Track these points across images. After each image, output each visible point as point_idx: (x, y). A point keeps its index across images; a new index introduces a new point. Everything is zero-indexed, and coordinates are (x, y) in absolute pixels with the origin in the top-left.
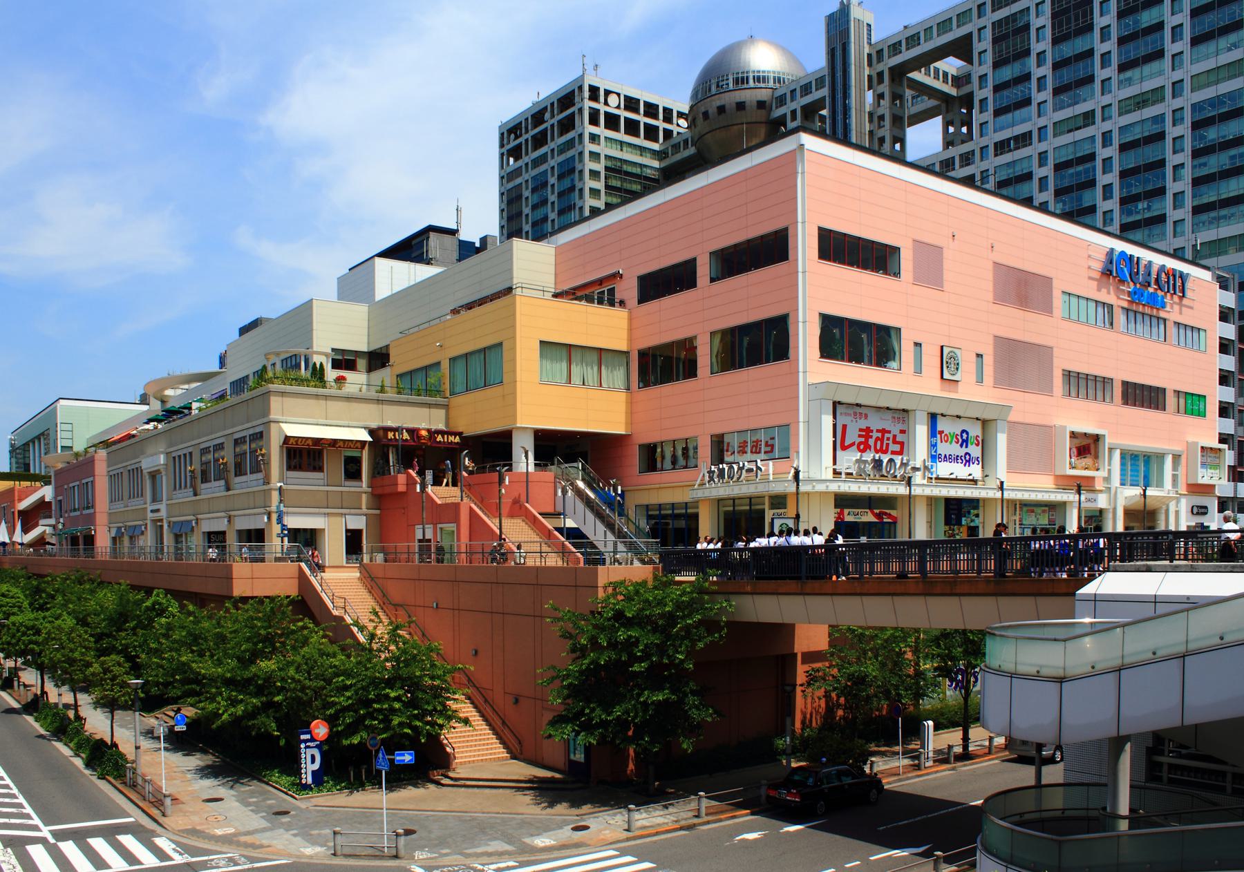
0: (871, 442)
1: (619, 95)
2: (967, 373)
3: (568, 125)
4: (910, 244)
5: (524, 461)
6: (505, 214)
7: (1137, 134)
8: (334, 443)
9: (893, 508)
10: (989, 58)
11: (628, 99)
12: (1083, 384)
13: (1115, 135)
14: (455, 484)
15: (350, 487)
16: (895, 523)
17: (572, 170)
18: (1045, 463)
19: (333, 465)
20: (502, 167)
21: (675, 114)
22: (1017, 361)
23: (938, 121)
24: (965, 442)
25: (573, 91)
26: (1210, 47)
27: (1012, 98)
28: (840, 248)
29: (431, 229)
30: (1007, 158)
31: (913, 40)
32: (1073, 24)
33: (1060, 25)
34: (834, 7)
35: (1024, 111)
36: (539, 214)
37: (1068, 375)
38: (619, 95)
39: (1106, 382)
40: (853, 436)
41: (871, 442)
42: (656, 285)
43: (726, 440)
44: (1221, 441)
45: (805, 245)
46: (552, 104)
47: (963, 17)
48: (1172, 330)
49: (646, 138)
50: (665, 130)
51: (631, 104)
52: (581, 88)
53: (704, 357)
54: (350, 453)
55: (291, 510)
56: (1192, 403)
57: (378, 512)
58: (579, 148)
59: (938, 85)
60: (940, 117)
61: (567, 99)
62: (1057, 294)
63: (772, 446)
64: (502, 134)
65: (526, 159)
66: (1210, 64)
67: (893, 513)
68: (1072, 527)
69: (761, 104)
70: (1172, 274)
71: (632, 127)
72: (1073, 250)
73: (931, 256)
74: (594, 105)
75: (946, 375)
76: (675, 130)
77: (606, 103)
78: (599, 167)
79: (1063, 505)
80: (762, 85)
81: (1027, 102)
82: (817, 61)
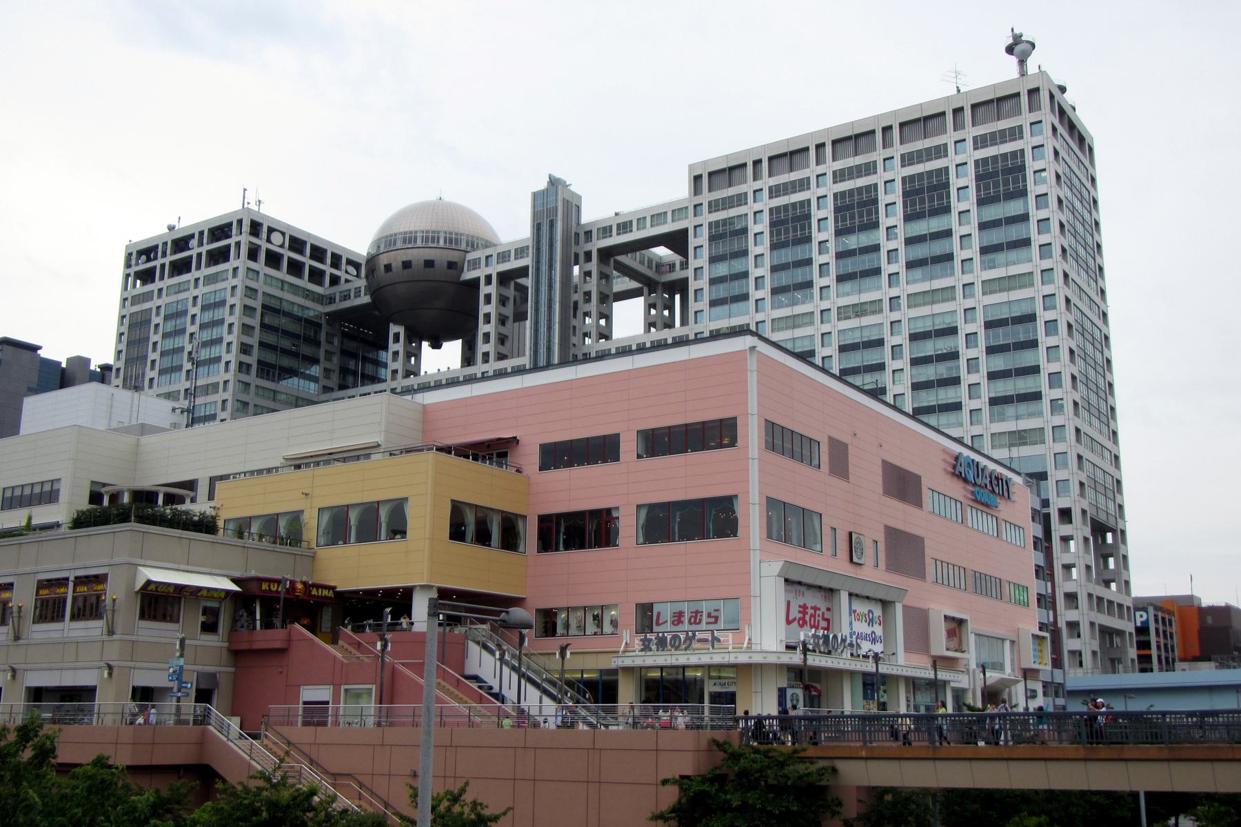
0: (807, 618)
1: (283, 234)
2: (868, 558)
4: (826, 441)
6: (124, 338)
8: (196, 591)
9: (819, 681)
10: (705, 253)
15: (210, 640)
16: (819, 696)
20: (126, 288)
21: (344, 261)
24: (871, 622)
25: (231, 224)
31: (625, 227)
32: (791, 234)
34: (542, 185)
35: (741, 305)
36: (169, 344)
38: (283, 234)
41: (807, 618)
43: (656, 609)
44: (1041, 629)
45: (752, 435)
46: (201, 233)
47: (679, 212)
50: (332, 275)
51: (297, 244)
52: (240, 222)
53: (628, 526)
54: (210, 604)
55: (138, 664)
57: (232, 669)
60: (642, 299)
63: (717, 618)
64: (130, 254)
65: (158, 284)
66: (925, 286)
67: (818, 686)
71: (295, 268)
73: (839, 452)
75: (855, 559)
76: (344, 276)
77: (269, 240)
80: (454, 246)
81: (745, 297)
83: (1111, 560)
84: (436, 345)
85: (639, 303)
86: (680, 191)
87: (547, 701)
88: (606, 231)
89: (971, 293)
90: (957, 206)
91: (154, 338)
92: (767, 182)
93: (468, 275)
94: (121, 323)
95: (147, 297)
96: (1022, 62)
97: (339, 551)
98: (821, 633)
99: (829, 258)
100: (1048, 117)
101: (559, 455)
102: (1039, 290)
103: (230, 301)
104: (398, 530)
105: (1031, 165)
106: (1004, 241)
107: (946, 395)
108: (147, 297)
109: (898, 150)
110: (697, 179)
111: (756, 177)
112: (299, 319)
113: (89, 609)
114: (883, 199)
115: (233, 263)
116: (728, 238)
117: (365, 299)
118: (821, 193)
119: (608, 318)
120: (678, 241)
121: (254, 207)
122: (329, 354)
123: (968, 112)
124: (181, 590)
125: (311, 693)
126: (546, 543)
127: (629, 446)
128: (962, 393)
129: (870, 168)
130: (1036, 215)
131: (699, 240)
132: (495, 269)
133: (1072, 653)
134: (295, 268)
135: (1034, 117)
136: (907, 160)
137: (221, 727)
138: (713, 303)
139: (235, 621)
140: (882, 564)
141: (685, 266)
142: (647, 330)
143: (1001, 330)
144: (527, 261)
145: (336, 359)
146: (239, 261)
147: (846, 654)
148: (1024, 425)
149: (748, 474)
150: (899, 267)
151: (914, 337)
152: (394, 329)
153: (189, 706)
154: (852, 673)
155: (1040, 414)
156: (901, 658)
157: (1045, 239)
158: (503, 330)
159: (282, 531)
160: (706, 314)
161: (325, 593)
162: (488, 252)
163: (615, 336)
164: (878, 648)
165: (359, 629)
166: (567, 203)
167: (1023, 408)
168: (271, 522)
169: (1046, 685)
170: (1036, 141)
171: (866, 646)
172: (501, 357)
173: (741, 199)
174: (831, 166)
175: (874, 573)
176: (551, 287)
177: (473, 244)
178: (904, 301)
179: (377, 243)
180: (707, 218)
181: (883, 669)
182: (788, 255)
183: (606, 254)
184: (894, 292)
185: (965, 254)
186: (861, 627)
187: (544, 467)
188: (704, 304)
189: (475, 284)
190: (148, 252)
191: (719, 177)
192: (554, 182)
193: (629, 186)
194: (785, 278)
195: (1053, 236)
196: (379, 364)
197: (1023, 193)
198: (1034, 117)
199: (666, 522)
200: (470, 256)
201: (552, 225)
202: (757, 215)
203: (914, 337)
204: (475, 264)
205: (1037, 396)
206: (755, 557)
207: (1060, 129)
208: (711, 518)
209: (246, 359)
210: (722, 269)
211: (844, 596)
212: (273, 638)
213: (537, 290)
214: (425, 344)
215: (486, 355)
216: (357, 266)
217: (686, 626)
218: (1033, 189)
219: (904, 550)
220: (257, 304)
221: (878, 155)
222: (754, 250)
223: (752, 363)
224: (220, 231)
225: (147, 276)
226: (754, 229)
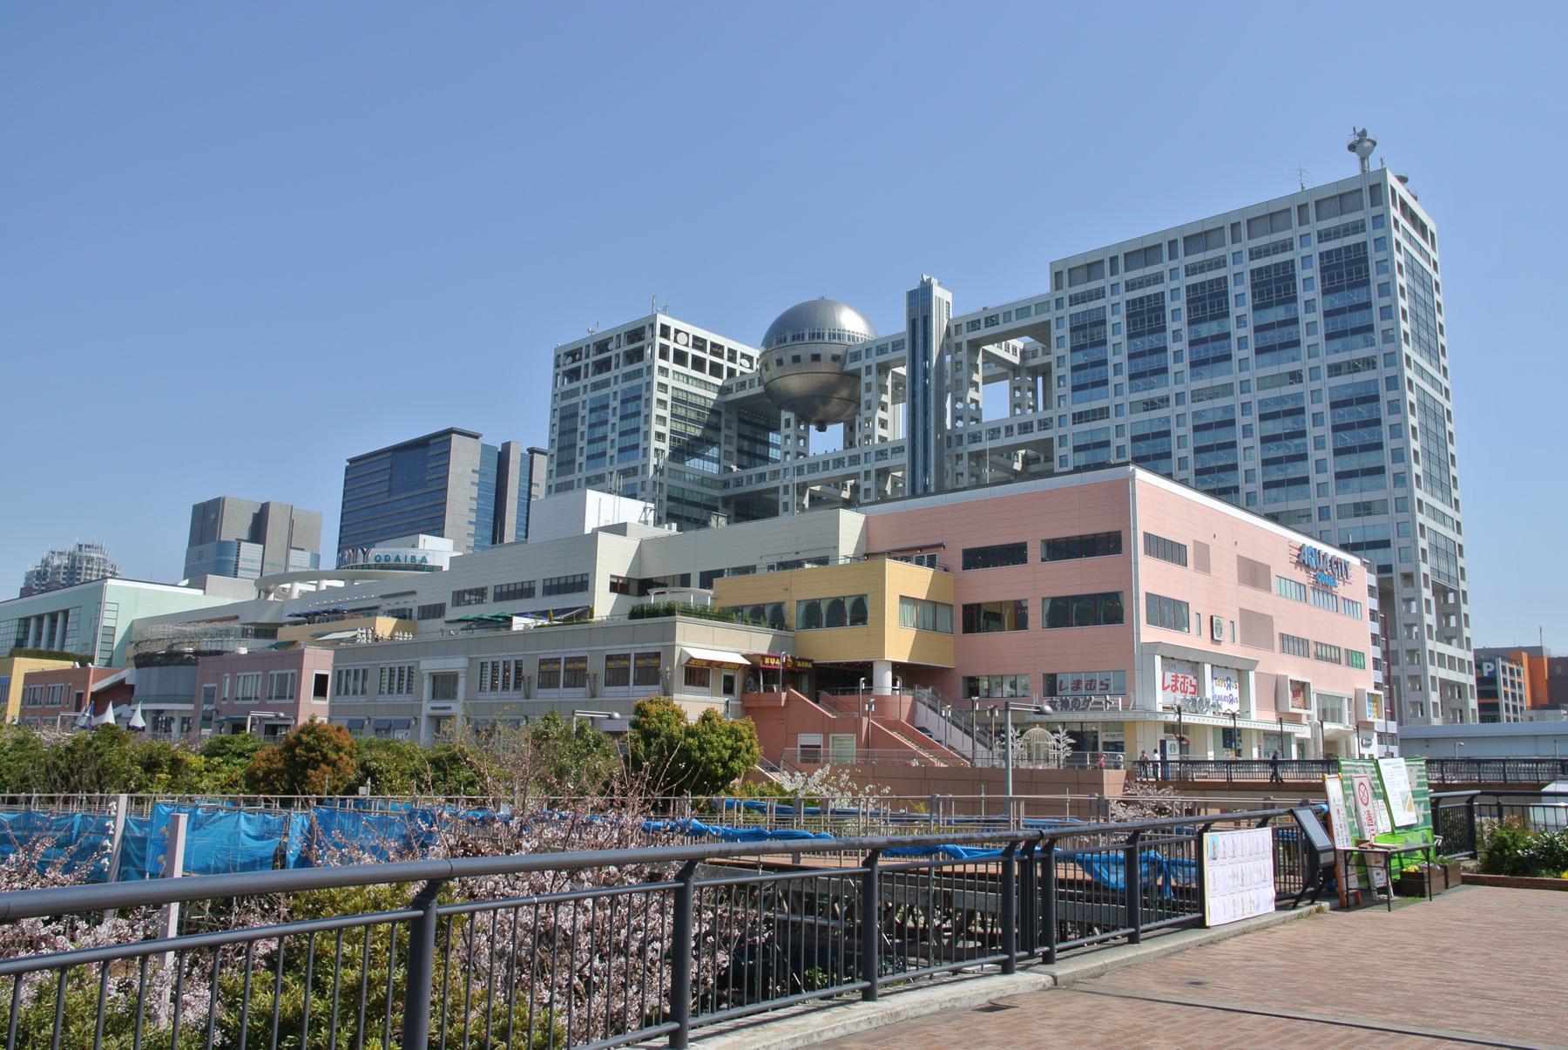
2: (1226, 636)
3: (637, 355)
5: (885, 682)
6: (557, 429)
7: (1209, 419)
8: (720, 665)
11: (696, 338)
14: (517, 686)
17: (639, 397)
19: (717, 681)
27: (1090, 378)
29: (451, 431)
30: (1085, 427)
31: (991, 321)
33: (1135, 324)
34: (916, 285)
37: (1282, 636)
39: (1305, 642)
42: (977, 558)
47: (1041, 306)
48: (1341, 603)
49: (711, 374)
52: (652, 326)
53: (1036, 615)
56: (1353, 659)
58: (648, 379)
59: (1009, 357)
61: (636, 334)
62: (1273, 577)
66: (1273, 370)
69: (835, 358)
70: (1336, 562)
71: (698, 364)
72: (1276, 542)
73: (1203, 550)
76: (738, 369)
78: (667, 397)
82: (898, 325)
83: (1453, 619)
84: (822, 428)
86: (1041, 286)
87: (979, 747)
94: (553, 416)
95: (575, 392)
97: (813, 633)
98: (1189, 697)
99: (1183, 345)
107: (1294, 471)
108: (575, 392)
110: (1057, 276)
117: (758, 390)
118: (1174, 286)
125: (806, 739)
133: (1414, 704)
139: (745, 685)
140: (1238, 639)
141: (1047, 352)
142: (1013, 414)
147: (1210, 713)
148: (1367, 497)
154: (1214, 727)
155: (1383, 487)
156: (1254, 713)
161: (807, 665)
164: (1235, 708)
167: (1367, 480)
169: (1380, 735)
171: (1225, 706)
180: (1069, 310)
181: (1240, 724)
182: (1144, 343)
184: (1244, 376)
186: (1221, 690)
187: (966, 566)
188: (1066, 390)
190: (573, 354)
191: (1079, 274)
194: (1143, 364)
196: (767, 444)
199: (1063, 612)
205: (1380, 470)
211: (1208, 668)
214: (812, 428)
217: (1083, 691)
222: (1112, 339)
225: (573, 375)
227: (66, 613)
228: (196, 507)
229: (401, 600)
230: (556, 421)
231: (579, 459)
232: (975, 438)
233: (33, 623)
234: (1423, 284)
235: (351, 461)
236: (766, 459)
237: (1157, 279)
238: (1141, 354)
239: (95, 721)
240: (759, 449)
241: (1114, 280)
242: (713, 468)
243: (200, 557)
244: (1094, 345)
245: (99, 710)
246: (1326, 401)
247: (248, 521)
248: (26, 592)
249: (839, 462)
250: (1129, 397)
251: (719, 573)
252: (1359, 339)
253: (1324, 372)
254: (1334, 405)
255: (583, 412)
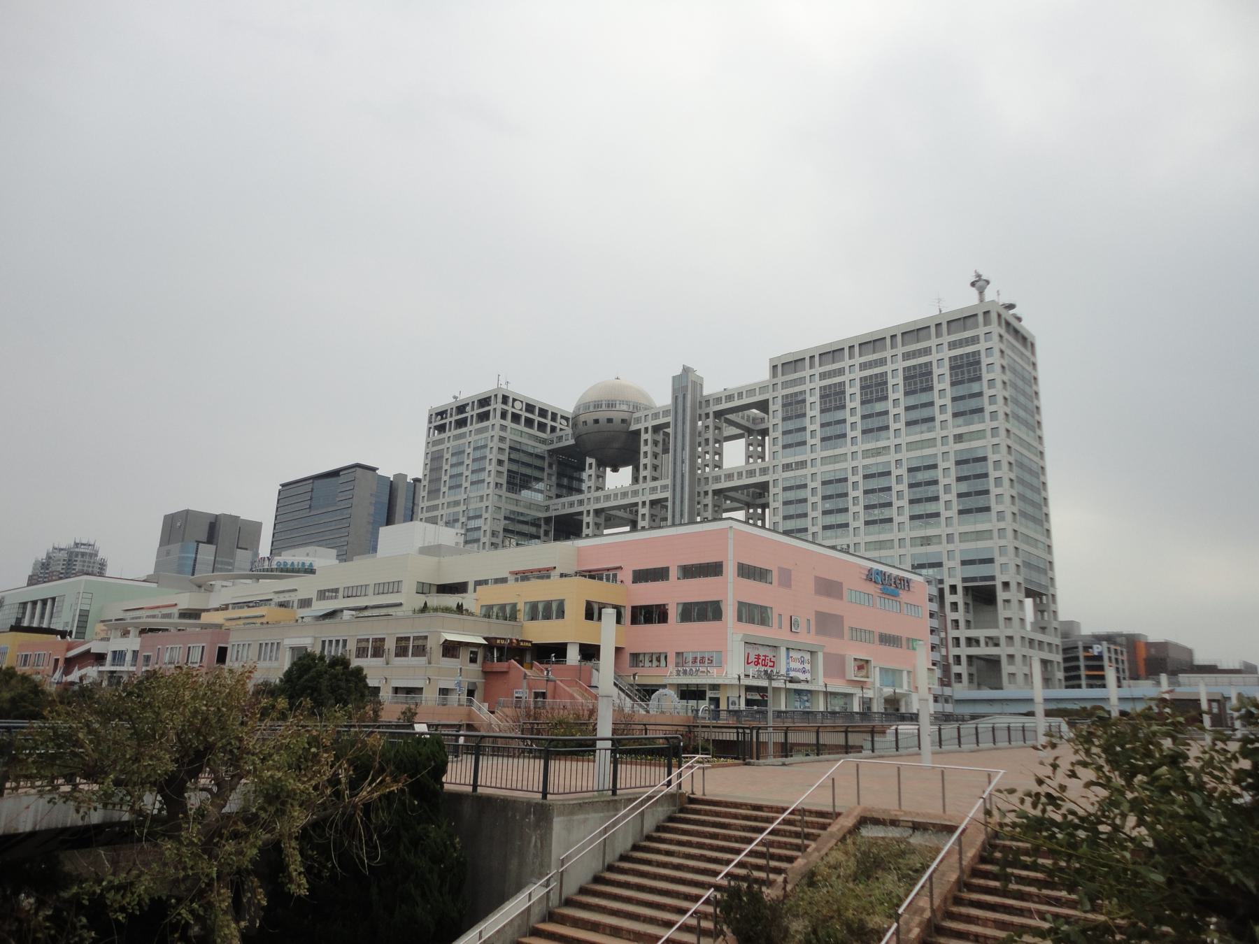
2: (802, 629)
10: (780, 415)
12: (859, 634)
13: (860, 469)
15: (473, 666)
18: (842, 674)
19: (465, 655)
22: (827, 623)
23: (742, 442)
24: (803, 662)
26: (917, 428)
28: (746, 571)
31: (730, 398)
33: (957, 375)
34: (679, 371)
36: (455, 471)
40: (752, 658)
45: (730, 570)
47: (763, 388)
51: (530, 408)
53: (673, 613)
65: (447, 434)
66: (917, 438)
68: (856, 708)
70: (902, 579)
71: (529, 422)
74: (504, 407)
79: (851, 695)
84: (615, 470)
85: (741, 443)
86: (764, 375)
88: (718, 400)
89: (943, 442)
90: (937, 386)
91: (445, 467)
92: (818, 370)
93: (634, 427)
95: (441, 441)
96: (981, 292)
100: (995, 328)
101: (642, 576)
102: (989, 441)
103: (490, 445)
104: (561, 614)
105: (985, 361)
106: (968, 408)
108: (441, 441)
109: (900, 350)
110: (775, 367)
111: (811, 367)
112: (531, 454)
113: (420, 651)
114: (891, 381)
115: (492, 421)
116: (794, 406)
117: (572, 442)
118: (852, 377)
119: (720, 454)
120: (763, 406)
121: (504, 386)
122: (550, 466)
123: (944, 326)
124: (460, 644)
126: (634, 621)
127: (674, 573)
128: (940, 507)
129: (882, 362)
130: (988, 392)
131: (776, 406)
132: (651, 423)
134: (529, 422)
135: (987, 329)
136: (907, 356)
137: (480, 709)
138: (785, 447)
139: (485, 658)
142: (747, 462)
143: (965, 466)
144: (669, 419)
145: (554, 478)
146: (495, 420)
149: (729, 590)
150: (901, 425)
151: (910, 470)
152: (589, 460)
153: (464, 697)
157: (993, 408)
158: (656, 462)
159: (508, 613)
160: (780, 454)
162: (646, 412)
163: (725, 466)
165: (160, 898)
166: (694, 383)
168: (503, 607)
170: (988, 345)
172: (655, 479)
173: (801, 381)
174: (858, 360)
175: (807, 638)
176: (683, 436)
177: (637, 407)
178: (904, 447)
179: (578, 408)
183: (718, 414)
185: (943, 417)
189: (638, 433)
190: (442, 414)
191: (787, 366)
192: (686, 370)
193: (734, 371)
194: (829, 431)
195: (999, 407)
196: (581, 481)
197: (979, 378)
198: (987, 329)
200: (635, 415)
201: (684, 397)
202: (812, 389)
203: (910, 470)
204: (638, 420)
206: (730, 631)
207: (1006, 336)
208: (708, 611)
209: (500, 469)
210: (791, 425)
212: (502, 666)
213: (676, 433)
214: (608, 470)
215: (645, 478)
216: (567, 419)
218: (986, 377)
219: (827, 623)
220: (506, 446)
221: (887, 354)
222: (810, 413)
223: (731, 535)
224: (484, 402)
225: (441, 428)
226: (809, 399)
227: (54, 599)
228: (166, 517)
229: (287, 595)
230: (428, 461)
231: (443, 489)
232: (717, 479)
233: (29, 606)
234: (1023, 379)
235: (283, 485)
236: (580, 491)
237: (841, 372)
238: (829, 424)
239: (64, 679)
240: (575, 484)
241: (812, 372)
242: (539, 497)
243: (168, 553)
244: (798, 416)
245: (67, 671)
246: (905, 468)
247: (206, 528)
248: (33, 581)
249: (625, 494)
250: (820, 454)
251: (486, 582)
252: (925, 426)
253: (951, 439)
254: (958, 463)
255: (447, 456)
